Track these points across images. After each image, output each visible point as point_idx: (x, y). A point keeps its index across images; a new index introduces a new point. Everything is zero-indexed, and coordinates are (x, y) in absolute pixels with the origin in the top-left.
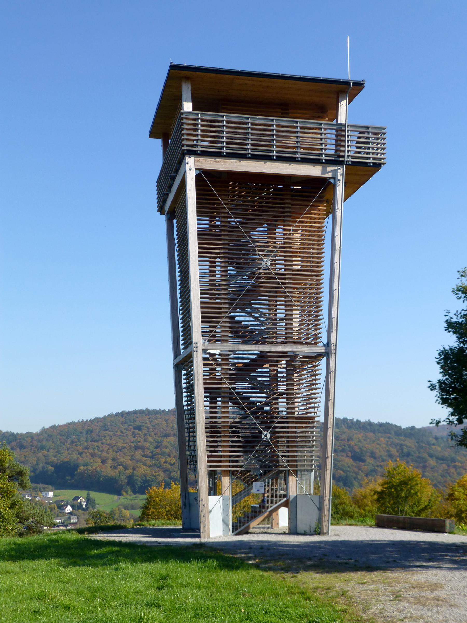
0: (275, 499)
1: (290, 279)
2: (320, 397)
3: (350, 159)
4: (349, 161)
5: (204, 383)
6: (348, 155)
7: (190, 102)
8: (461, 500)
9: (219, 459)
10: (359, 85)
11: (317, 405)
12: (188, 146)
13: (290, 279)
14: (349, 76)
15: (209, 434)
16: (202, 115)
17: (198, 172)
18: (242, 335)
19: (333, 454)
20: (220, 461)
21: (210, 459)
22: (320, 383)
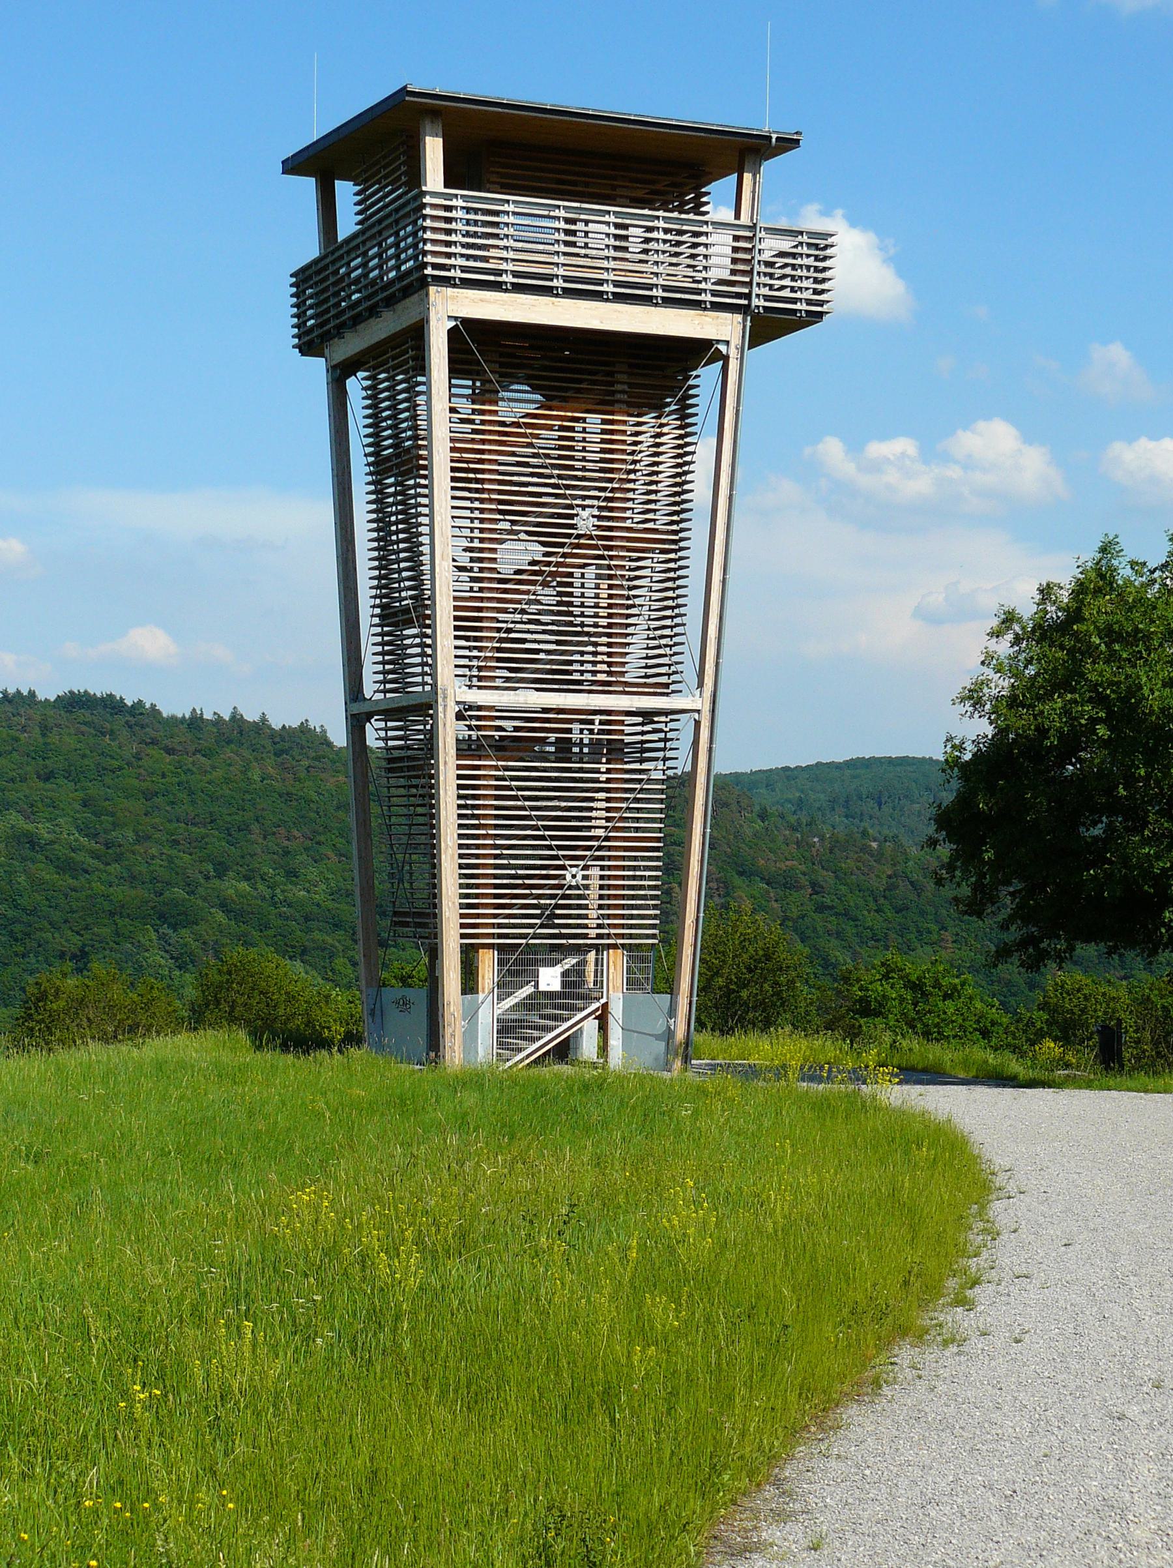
0: (579, 1003)
1: (623, 548)
2: (696, 444)
3: (762, 303)
4: (758, 307)
5: (452, 477)
6: (759, 292)
7: (437, 136)
8: (974, 1340)
9: (476, 614)
10: (788, 144)
11: (688, 458)
12: (435, 266)
13: (623, 548)
14: (767, 124)
15: (462, 881)
16: (460, 198)
17: (452, 324)
18: (524, 1073)
19: (702, 915)
20: (480, 609)
21: (461, 792)
22: (696, 424)
